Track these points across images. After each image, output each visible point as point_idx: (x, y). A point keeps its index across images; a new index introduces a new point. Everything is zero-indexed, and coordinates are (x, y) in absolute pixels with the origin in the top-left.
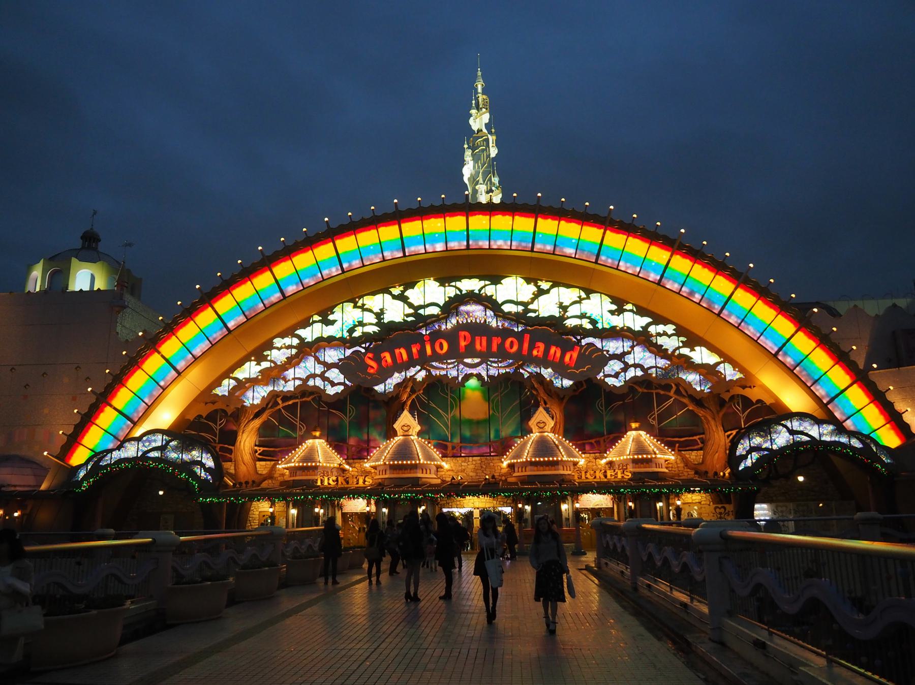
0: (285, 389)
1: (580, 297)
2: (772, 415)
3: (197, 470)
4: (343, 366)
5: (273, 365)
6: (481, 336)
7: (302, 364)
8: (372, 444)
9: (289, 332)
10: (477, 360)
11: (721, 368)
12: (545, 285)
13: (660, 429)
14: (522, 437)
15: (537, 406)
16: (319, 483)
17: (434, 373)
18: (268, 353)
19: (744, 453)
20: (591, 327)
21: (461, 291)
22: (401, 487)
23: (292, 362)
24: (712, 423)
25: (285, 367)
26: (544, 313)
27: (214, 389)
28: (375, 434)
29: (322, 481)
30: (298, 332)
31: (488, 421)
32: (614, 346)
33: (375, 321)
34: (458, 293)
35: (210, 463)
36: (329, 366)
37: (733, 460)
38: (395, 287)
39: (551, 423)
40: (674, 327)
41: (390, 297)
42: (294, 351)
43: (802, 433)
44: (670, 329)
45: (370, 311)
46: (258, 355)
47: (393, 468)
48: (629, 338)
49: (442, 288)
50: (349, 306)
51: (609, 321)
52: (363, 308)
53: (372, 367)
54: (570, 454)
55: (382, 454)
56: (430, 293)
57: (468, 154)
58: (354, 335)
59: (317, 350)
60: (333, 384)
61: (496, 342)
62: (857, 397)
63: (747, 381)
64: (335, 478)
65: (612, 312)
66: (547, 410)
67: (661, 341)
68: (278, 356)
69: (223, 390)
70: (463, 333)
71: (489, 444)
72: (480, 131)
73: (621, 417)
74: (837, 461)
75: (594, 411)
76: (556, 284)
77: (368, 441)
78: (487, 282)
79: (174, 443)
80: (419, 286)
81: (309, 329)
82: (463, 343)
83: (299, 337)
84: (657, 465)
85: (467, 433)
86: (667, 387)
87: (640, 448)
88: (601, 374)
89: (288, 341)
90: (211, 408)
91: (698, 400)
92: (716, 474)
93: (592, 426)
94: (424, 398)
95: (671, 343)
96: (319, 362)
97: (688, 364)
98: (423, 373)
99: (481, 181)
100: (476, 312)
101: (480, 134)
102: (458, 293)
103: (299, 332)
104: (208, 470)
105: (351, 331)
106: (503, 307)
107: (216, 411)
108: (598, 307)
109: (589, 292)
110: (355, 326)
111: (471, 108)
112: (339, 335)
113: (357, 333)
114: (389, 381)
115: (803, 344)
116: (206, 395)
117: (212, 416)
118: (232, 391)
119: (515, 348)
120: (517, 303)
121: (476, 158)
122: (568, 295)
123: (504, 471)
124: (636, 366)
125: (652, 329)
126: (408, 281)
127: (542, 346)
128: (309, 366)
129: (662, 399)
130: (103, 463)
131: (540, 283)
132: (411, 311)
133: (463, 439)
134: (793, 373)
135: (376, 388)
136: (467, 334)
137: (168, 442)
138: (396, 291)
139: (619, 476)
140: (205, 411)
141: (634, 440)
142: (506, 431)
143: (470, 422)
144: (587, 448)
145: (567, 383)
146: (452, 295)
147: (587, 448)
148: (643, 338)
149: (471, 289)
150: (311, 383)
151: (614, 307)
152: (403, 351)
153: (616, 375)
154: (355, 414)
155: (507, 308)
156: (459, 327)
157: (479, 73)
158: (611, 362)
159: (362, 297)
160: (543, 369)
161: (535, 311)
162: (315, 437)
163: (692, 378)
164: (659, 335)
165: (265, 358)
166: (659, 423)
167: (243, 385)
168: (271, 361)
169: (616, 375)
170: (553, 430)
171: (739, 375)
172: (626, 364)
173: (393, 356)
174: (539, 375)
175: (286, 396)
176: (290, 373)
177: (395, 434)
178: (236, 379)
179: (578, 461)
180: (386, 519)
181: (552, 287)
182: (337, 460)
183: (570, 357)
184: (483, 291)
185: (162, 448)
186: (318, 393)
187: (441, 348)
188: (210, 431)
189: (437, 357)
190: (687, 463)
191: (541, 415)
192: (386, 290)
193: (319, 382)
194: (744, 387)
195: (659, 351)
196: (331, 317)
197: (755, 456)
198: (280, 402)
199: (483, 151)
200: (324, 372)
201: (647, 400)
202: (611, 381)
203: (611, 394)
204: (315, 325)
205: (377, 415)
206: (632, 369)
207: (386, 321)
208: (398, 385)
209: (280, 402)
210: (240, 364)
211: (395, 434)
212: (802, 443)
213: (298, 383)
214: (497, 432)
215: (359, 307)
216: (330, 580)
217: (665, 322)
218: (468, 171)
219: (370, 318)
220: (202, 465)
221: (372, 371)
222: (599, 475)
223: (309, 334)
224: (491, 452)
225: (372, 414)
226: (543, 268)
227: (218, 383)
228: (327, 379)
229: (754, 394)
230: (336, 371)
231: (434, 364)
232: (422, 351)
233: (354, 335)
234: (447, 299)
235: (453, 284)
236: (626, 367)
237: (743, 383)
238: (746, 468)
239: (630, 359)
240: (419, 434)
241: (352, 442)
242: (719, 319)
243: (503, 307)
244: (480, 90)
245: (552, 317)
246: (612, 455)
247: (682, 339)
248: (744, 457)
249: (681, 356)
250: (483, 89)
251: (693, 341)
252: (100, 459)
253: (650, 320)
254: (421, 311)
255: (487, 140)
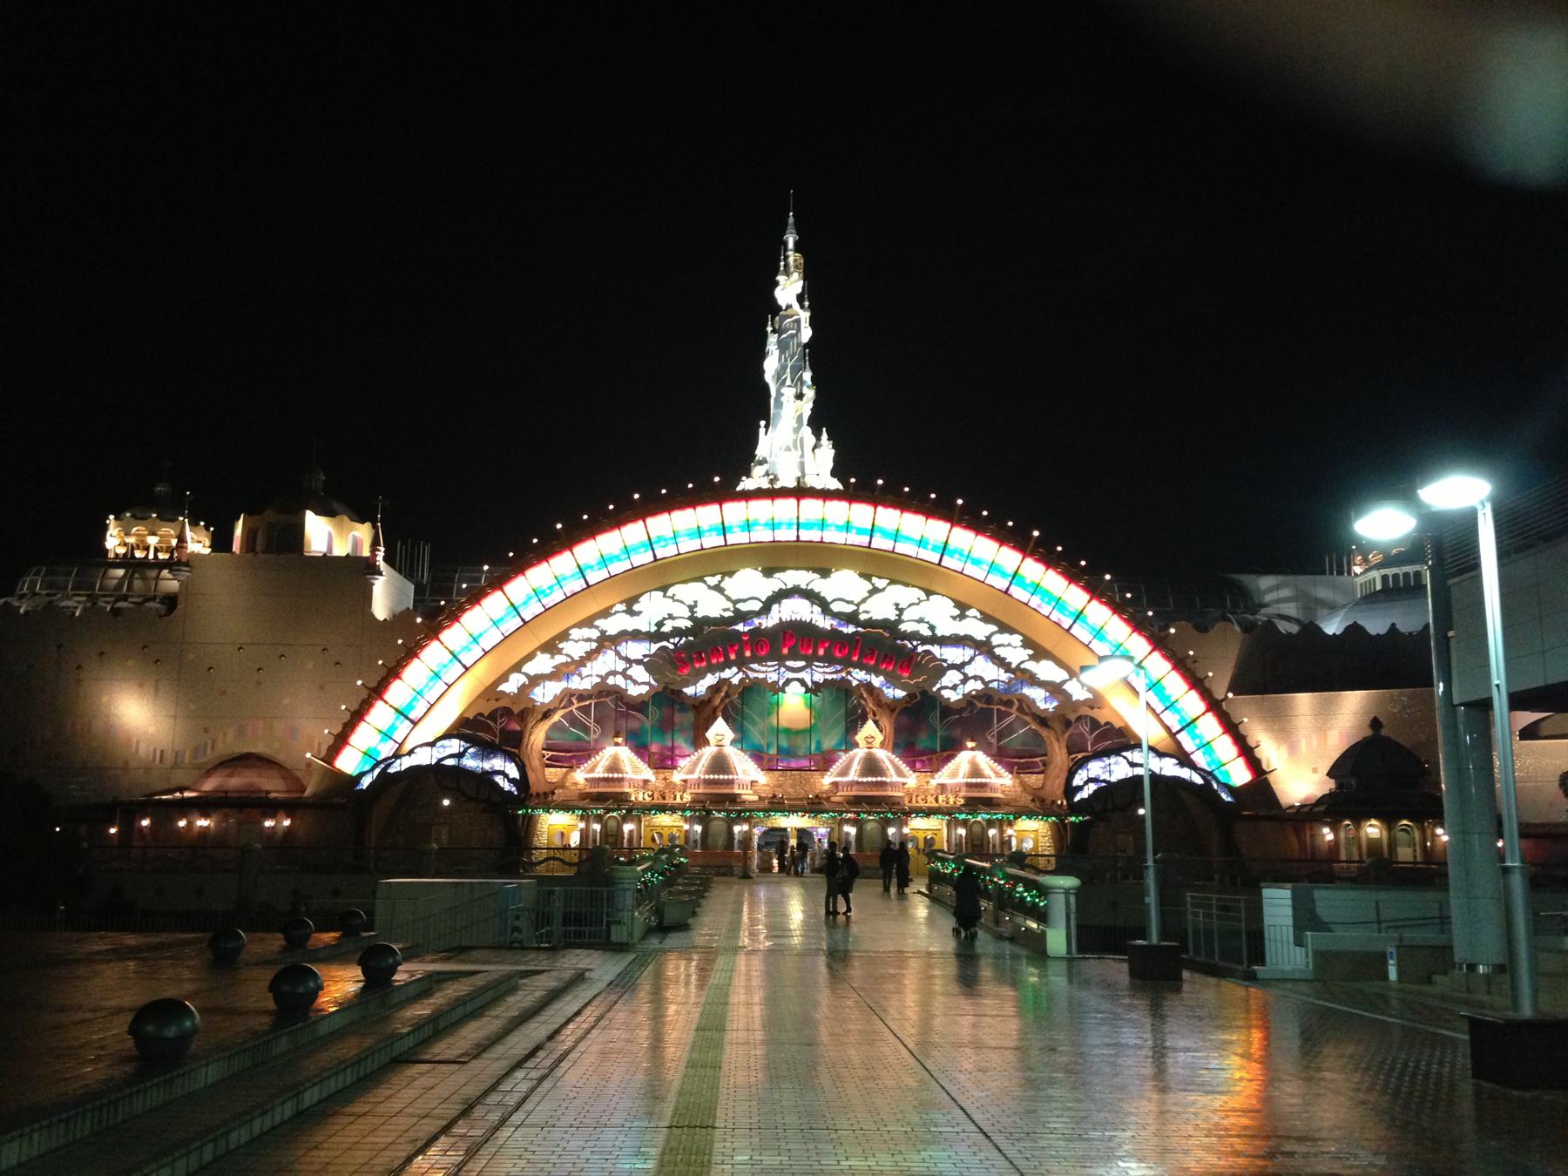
2: (1119, 740)
3: (499, 779)
4: (651, 664)
8: (677, 752)
9: (588, 622)
13: (999, 748)
14: (846, 751)
15: (864, 720)
22: (717, 801)
23: (590, 656)
24: (1056, 745)
25: (582, 662)
26: (877, 615)
30: (597, 623)
31: (810, 731)
32: (953, 655)
35: (513, 772)
37: (1070, 791)
39: (880, 737)
42: (594, 645)
44: (1016, 639)
46: (550, 647)
47: (708, 783)
51: (946, 628)
54: (900, 773)
55: (691, 769)
56: (749, 585)
57: (772, 339)
60: (635, 682)
62: (1210, 726)
65: (954, 618)
66: (876, 723)
68: (574, 649)
69: (511, 686)
71: (810, 757)
72: (789, 307)
73: (957, 733)
74: (1184, 795)
75: (928, 727)
76: (893, 582)
77: (673, 749)
79: (471, 750)
84: (993, 789)
85: (784, 743)
86: (1009, 703)
87: (975, 771)
90: (493, 705)
91: (1043, 720)
92: (1053, 802)
93: (923, 742)
94: (738, 702)
96: (621, 658)
97: (1033, 680)
98: (741, 675)
99: (788, 382)
101: (789, 312)
104: (511, 781)
105: (660, 624)
109: (929, 593)
111: (777, 272)
113: (666, 629)
117: (493, 716)
118: (523, 689)
121: (783, 346)
124: (976, 678)
125: (996, 640)
126: (726, 570)
128: (607, 662)
129: (1002, 716)
130: (391, 770)
133: (779, 749)
137: (465, 750)
138: (713, 581)
139: (951, 801)
141: (972, 765)
142: (828, 744)
143: (788, 731)
144: (918, 765)
147: (918, 765)
148: (985, 648)
150: (611, 681)
151: (957, 612)
153: (954, 688)
154: (664, 718)
155: (836, 607)
157: (791, 220)
158: (950, 673)
162: (617, 744)
163: (1037, 695)
165: (560, 651)
166: (999, 740)
167: (535, 680)
169: (954, 688)
170: (882, 745)
172: (965, 675)
174: (870, 684)
175: (582, 696)
177: (707, 742)
178: (526, 675)
179: (904, 779)
180: (698, 838)
182: (647, 773)
185: (460, 755)
186: (618, 694)
188: (488, 729)
190: (1023, 784)
191: (869, 728)
192: (700, 579)
193: (619, 681)
195: (1001, 662)
197: (1092, 787)
199: (792, 336)
201: (986, 716)
202: (946, 694)
203: (947, 709)
205: (685, 719)
208: (710, 688)
211: (707, 742)
216: (893, 890)
217: (1012, 631)
218: (771, 365)
220: (506, 775)
222: (931, 799)
225: (678, 717)
226: (878, 564)
227: (504, 678)
228: (630, 678)
229: (1102, 716)
230: (641, 668)
236: (965, 680)
238: (1082, 800)
240: (733, 742)
241: (654, 748)
242: (1067, 636)
244: (791, 245)
245: (886, 621)
246: (944, 776)
248: (1080, 788)
249: (1025, 671)
250: (796, 244)
251: (1040, 653)
252: (388, 766)
254: (741, 606)
255: (798, 321)
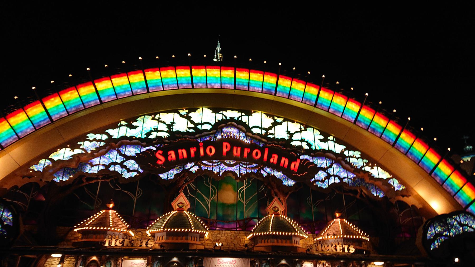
0: (90, 172)
1: (300, 129)
4: (138, 158)
5: (83, 152)
6: (237, 146)
7: (107, 156)
10: (232, 162)
11: (391, 182)
12: (279, 120)
16: (107, 244)
17: (203, 169)
18: (82, 143)
19: (432, 238)
20: (308, 148)
21: (226, 117)
23: (99, 152)
27: (104, 145)
28: (155, 210)
29: (110, 243)
32: (320, 162)
33: (166, 129)
34: (224, 118)
36: (128, 158)
38: (183, 110)
40: (360, 153)
41: (178, 115)
42: (102, 144)
43: (467, 225)
44: (357, 154)
45: (164, 123)
47: (169, 234)
48: (330, 158)
49: (214, 114)
50: (148, 119)
52: (158, 120)
53: (161, 160)
56: (205, 116)
58: (150, 137)
59: (121, 146)
60: (129, 171)
61: (246, 151)
63: (407, 192)
64: (121, 240)
67: (352, 160)
68: (88, 146)
70: (225, 144)
78: (243, 114)
80: (199, 111)
81: (116, 130)
82: (225, 150)
83: (108, 134)
88: (313, 179)
89: (98, 136)
90: (27, 181)
95: (359, 163)
96: (121, 154)
100: (233, 132)
102: (224, 118)
103: (109, 131)
105: (149, 134)
106: (252, 130)
107: (31, 184)
108: (312, 137)
109: (306, 127)
110: (152, 131)
112: (139, 136)
113: (152, 137)
114: (171, 172)
115: (444, 170)
116: (23, 170)
117: (26, 188)
118: (46, 169)
119: (259, 156)
120: (261, 128)
122: (294, 127)
123: (246, 242)
124: (335, 176)
127: (276, 157)
128: (114, 156)
131: (276, 118)
132: (193, 126)
134: (440, 186)
135: (161, 176)
136: (228, 145)
138: (183, 112)
140: (20, 182)
145: (291, 183)
146: (220, 119)
148: (339, 159)
149: (232, 117)
150: (112, 169)
151: (322, 137)
152: (184, 151)
153: (323, 181)
155: (255, 131)
156: (223, 140)
159: (159, 113)
160: (275, 172)
161: (272, 134)
164: (350, 157)
165: (78, 147)
168: (83, 149)
171: (402, 187)
173: (177, 154)
176: (96, 160)
178: (52, 160)
181: (283, 121)
183: (295, 165)
184: (240, 119)
187: (211, 151)
189: (206, 157)
191: (276, 203)
192: (177, 111)
193: (118, 169)
194: (403, 196)
196: (134, 124)
198: (85, 181)
200: (124, 161)
202: (319, 184)
204: (121, 127)
206: (333, 177)
207: (174, 130)
209: (85, 181)
210: (55, 150)
212: (468, 233)
213: (101, 168)
214: (242, 213)
215: (156, 119)
219: (163, 127)
221: (160, 163)
223: (115, 133)
224: (237, 228)
227: (36, 161)
229: (410, 201)
230: (133, 162)
231: (204, 162)
232: (198, 152)
233: (150, 137)
234: (217, 121)
235: (221, 112)
236: (329, 177)
237: (405, 193)
239: (331, 171)
243: (252, 130)
245: (283, 139)
247: (365, 161)
248: (433, 241)
253: (345, 147)
254: (199, 127)
